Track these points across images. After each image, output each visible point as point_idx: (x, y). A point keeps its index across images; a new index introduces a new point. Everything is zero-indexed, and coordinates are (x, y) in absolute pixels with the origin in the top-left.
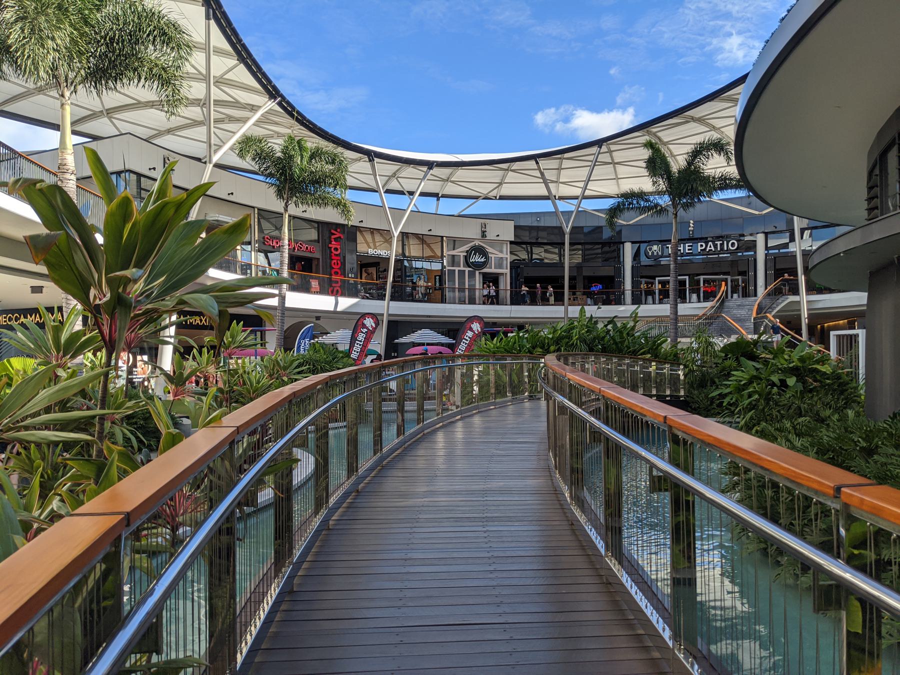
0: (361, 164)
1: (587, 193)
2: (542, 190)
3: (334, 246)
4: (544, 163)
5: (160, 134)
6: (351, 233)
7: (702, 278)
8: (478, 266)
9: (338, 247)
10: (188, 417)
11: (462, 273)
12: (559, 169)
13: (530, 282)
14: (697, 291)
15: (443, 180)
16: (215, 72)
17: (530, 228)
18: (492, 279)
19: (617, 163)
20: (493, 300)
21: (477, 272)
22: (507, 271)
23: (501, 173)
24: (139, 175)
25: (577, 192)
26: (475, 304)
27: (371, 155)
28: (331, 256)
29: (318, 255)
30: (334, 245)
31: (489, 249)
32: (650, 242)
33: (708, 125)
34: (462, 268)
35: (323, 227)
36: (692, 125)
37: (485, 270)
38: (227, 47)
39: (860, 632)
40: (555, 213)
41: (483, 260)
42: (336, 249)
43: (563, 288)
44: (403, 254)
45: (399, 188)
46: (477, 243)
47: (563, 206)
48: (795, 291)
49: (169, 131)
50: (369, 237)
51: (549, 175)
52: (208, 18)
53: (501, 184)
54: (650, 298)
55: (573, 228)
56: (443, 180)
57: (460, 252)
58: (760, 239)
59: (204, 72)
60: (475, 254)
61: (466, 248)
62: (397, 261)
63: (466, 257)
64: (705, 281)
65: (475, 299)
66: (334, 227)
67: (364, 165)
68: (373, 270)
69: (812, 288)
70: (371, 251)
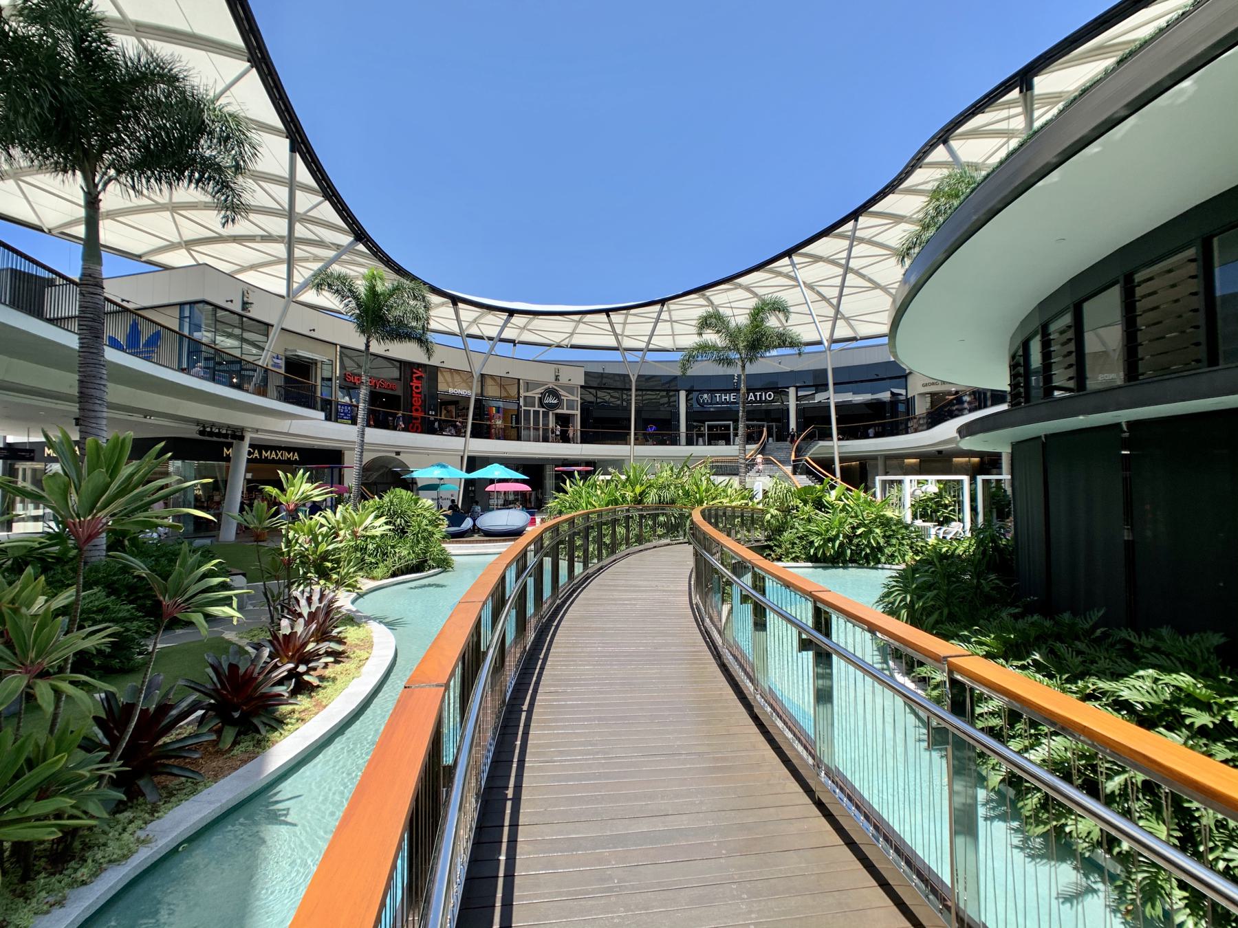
0: (443, 309)
1: (651, 346)
2: (612, 342)
4: (613, 316)
5: (243, 269)
6: (432, 372)
8: (552, 407)
10: (391, 625)
11: (537, 413)
12: (625, 323)
13: (602, 422)
16: (300, 208)
18: (564, 420)
20: (565, 438)
22: (578, 413)
23: (573, 324)
24: (216, 307)
25: (643, 345)
27: (455, 300)
29: (399, 392)
30: (414, 384)
31: (562, 392)
32: (702, 391)
33: (752, 292)
35: (407, 367)
36: (740, 291)
38: (313, 183)
39: (1017, 90)
42: (417, 388)
43: (830, 423)
44: (482, 395)
45: (478, 333)
47: (631, 357)
48: (827, 436)
49: (253, 267)
50: (448, 375)
51: (619, 330)
52: (293, 150)
53: (572, 334)
54: (701, 440)
57: (536, 393)
58: (792, 391)
59: (287, 207)
62: (476, 400)
67: (448, 311)
68: (452, 408)
69: (846, 434)
70: (451, 390)
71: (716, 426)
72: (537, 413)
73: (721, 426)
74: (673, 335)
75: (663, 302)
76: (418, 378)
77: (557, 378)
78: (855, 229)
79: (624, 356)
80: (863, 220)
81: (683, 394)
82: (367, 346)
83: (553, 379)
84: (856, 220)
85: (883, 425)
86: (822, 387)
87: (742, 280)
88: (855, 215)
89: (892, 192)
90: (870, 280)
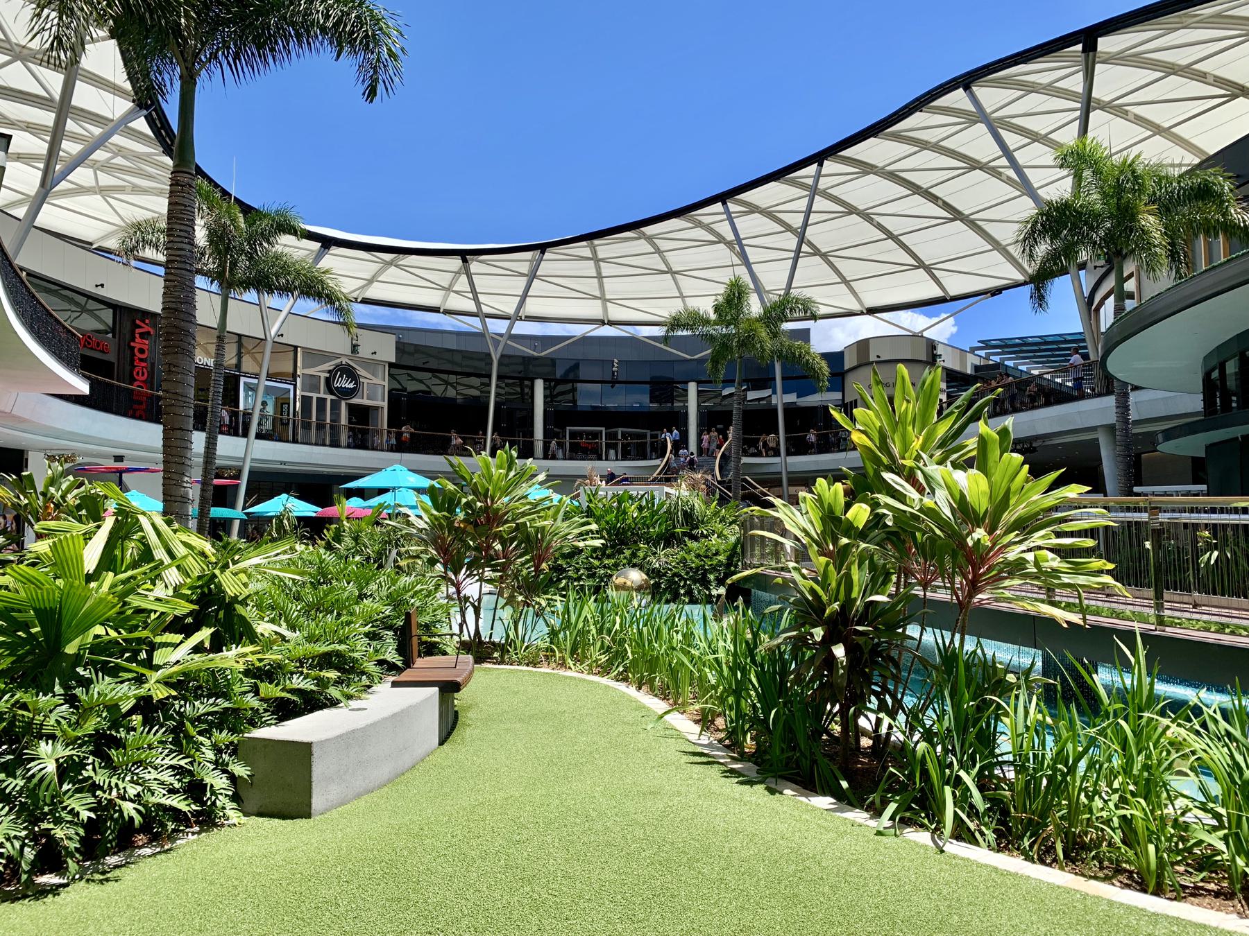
3: (138, 346)
7: (620, 430)
9: (145, 347)
11: (321, 402)
14: (615, 447)
15: (444, 288)
17: (418, 349)
18: (361, 415)
19: (609, 300)
21: (343, 404)
25: (510, 309)
26: (338, 446)
28: (132, 360)
31: (361, 372)
34: (322, 395)
37: (356, 401)
39: (1079, 47)
40: (481, 336)
41: (351, 386)
42: (142, 351)
46: (344, 360)
53: (370, 281)
54: (612, 452)
55: (502, 356)
56: (444, 288)
60: (341, 376)
61: (329, 366)
63: (327, 380)
64: (623, 434)
65: (339, 440)
66: (140, 315)
71: (580, 434)
72: (321, 402)
73: (588, 433)
74: (682, 297)
75: (543, 248)
76: (142, 336)
77: (355, 348)
78: (818, 176)
79: (484, 324)
80: (829, 166)
81: (539, 386)
82: (684, 302)
83: (347, 350)
84: (821, 165)
85: (609, 446)
86: (763, 380)
87: (649, 230)
88: (819, 158)
89: (875, 135)
90: (947, 206)
